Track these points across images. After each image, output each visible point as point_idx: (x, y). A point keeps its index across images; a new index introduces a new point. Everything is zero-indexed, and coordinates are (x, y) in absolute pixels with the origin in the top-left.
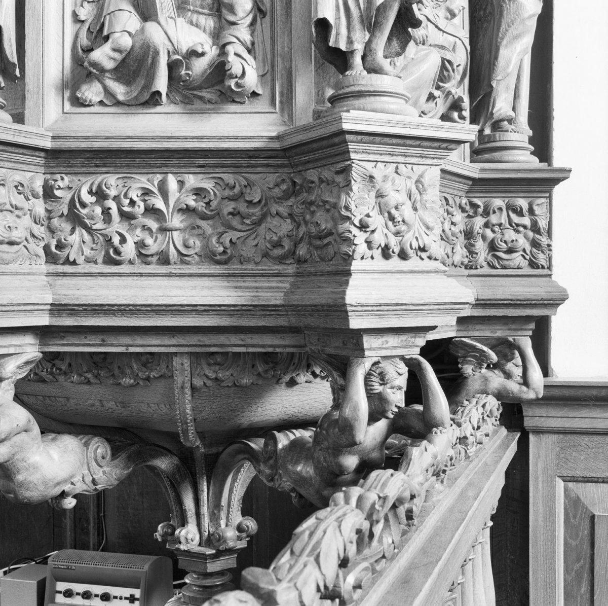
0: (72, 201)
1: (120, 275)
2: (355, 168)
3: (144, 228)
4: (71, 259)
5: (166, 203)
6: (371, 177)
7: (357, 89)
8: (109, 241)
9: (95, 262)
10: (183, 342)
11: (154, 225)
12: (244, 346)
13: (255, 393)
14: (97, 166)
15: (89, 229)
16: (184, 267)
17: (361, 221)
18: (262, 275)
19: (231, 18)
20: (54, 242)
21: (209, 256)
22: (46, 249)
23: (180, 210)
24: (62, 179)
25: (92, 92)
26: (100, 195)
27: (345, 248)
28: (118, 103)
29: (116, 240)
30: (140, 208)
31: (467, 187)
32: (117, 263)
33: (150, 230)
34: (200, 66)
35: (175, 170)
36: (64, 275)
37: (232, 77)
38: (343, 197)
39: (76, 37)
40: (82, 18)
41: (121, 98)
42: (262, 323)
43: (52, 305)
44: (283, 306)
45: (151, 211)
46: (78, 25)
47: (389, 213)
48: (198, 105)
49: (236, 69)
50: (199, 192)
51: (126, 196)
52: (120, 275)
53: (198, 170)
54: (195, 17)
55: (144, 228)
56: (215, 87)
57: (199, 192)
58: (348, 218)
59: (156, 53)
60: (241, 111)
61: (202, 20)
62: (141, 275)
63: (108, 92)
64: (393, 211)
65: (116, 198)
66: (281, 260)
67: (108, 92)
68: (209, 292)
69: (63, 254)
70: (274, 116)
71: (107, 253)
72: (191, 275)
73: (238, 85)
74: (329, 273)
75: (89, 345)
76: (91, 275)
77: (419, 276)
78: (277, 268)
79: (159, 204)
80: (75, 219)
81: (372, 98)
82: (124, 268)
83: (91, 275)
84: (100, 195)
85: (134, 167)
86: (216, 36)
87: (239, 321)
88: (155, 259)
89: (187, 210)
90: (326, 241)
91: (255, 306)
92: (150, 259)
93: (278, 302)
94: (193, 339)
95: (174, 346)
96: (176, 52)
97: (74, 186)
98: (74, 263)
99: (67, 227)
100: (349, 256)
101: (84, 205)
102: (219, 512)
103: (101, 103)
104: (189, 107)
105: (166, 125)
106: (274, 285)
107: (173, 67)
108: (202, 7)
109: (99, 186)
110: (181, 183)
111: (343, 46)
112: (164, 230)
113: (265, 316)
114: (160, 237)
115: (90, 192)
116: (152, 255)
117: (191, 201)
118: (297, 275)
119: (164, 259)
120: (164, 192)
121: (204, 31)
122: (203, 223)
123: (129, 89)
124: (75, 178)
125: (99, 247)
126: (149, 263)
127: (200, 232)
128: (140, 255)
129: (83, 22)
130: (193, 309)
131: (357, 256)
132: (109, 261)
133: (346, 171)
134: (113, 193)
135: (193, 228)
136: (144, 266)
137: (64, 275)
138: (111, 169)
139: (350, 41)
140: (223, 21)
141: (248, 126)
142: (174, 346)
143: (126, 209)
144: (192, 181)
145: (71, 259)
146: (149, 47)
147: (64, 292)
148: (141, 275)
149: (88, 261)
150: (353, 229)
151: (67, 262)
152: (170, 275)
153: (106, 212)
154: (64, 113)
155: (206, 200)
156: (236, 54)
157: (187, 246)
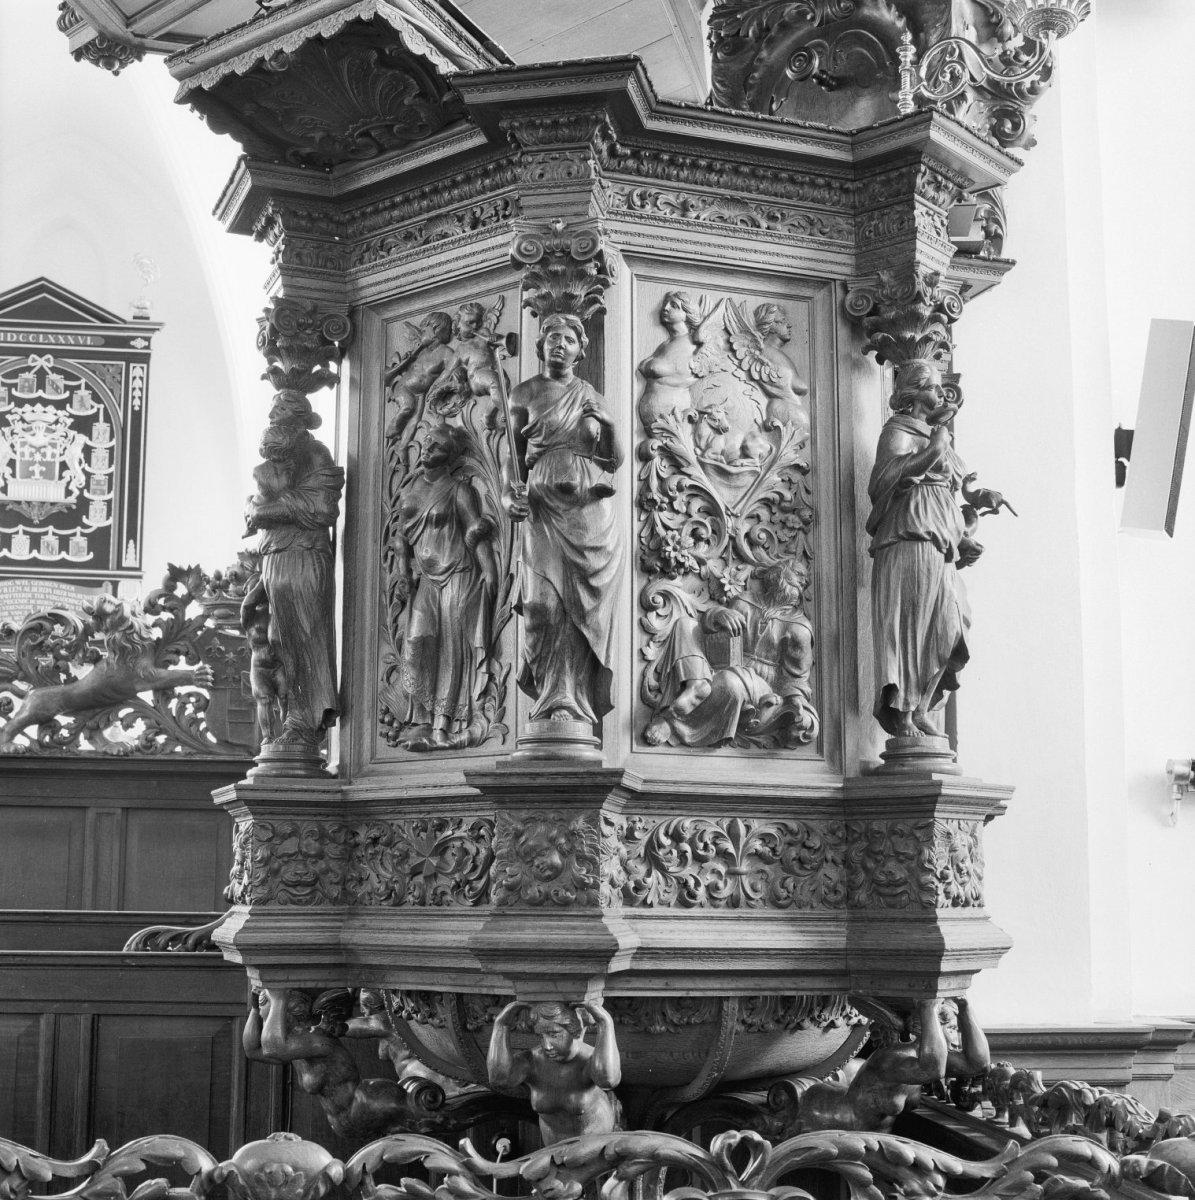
0: (650, 841)
1: (692, 918)
2: (937, 825)
3: (714, 871)
4: (649, 902)
5: (736, 844)
6: (949, 834)
7: (917, 750)
8: (685, 884)
9: (669, 905)
10: (741, 986)
11: (722, 869)
12: (794, 989)
13: (768, 1038)
14: (672, 809)
15: (663, 871)
16: (750, 910)
17: (942, 873)
18: (819, 920)
19: (797, 672)
20: (632, 885)
21: (774, 901)
22: (625, 890)
23: (750, 855)
24: (640, 820)
25: (661, 732)
26: (676, 837)
27: (926, 898)
28: (682, 743)
29: (692, 882)
30: (712, 854)
31: (623, 802)
32: (688, 905)
33: (719, 873)
34: (768, 714)
35: (742, 815)
36: (641, 917)
37: (801, 728)
38: (926, 851)
39: (643, 675)
40: (650, 657)
41: (688, 740)
42: (822, 966)
43: (639, 948)
44: (846, 950)
45: (723, 855)
46: (644, 664)
47: (958, 866)
48: (754, 750)
49: (807, 722)
50: (765, 838)
51: (701, 840)
52: (692, 918)
53: (764, 815)
54: (759, 666)
55: (714, 871)
56: (783, 734)
57: (765, 838)
58: (931, 870)
59: (735, 702)
60: (519, 708)
61: (766, 669)
62: (712, 918)
63: (675, 733)
64: (961, 865)
65: (692, 842)
66: (836, 905)
67: (675, 733)
68: (770, 935)
69: (641, 896)
70: (822, 763)
71: (680, 896)
72: (757, 919)
73: (805, 736)
74: (904, 920)
75: (653, 990)
76: (665, 918)
77: (974, 923)
78: (832, 912)
79: (729, 846)
80: (652, 859)
81: (939, 759)
82: (695, 911)
83: (665, 918)
84: (676, 837)
85: (706, 811)
86: (777, 686)
87: (801, 966)
88: (723, 903)
89: (758, 855)
90: (900, 890)
91: (821, 950)
92: (718, 902)
93: (842, 947)
94: (750, 983)
95: (732, 990)
96: (751, 702)
97: (650, 827)
98: (651, 905)
99: (642, 869)
100: (931, 904)
101: (661, 846)
102: (655, 1185)
103: (667, 743)
104: (747, 751)
105: (725, 769)
106: (832, 929)
107: (745, 714)
108: (767, 658)
109: (676, 828)
110: (748, 828)
111: (900, 707)
112: (733, 874)
113: (826, 959)
114: (730, 882)
115: (666, 834)
116: (720, 900)
117: (757, 845)
118: (852, 920)
119: (733, 902)
120: (734, 837)
121: (767, 680)
122: (767, 868)
123: (695, 731)
124: (650, 819)
125: (672, 889)
126: (715, 907)
127: (764, 877)
128: (711, 898)
129: (649, 662)
130: (767, 953)
131: (939, 905)
132: (683, 903)
133: (930, 826)
134: (687, 835)
135: (758, 872)
136: (712, 909)
137: (641, 917)
138: (684, 813)
139: (907, 703)
140: (784, 672)
141: (800, 774)
142: (732, 990)
143: (702, 853)
144: (757, 826)
145: (649, 902)
146: (729, 696)
147: (650, 936)
148: (712, 918)
149: (661, 903)
150: (935, 880)
151: (644, 903)
152: (738, 919)
153: (682, 855)
154: (632, 751)
155: (772, 846)
156: (805, 708)
157: (755, 890)
